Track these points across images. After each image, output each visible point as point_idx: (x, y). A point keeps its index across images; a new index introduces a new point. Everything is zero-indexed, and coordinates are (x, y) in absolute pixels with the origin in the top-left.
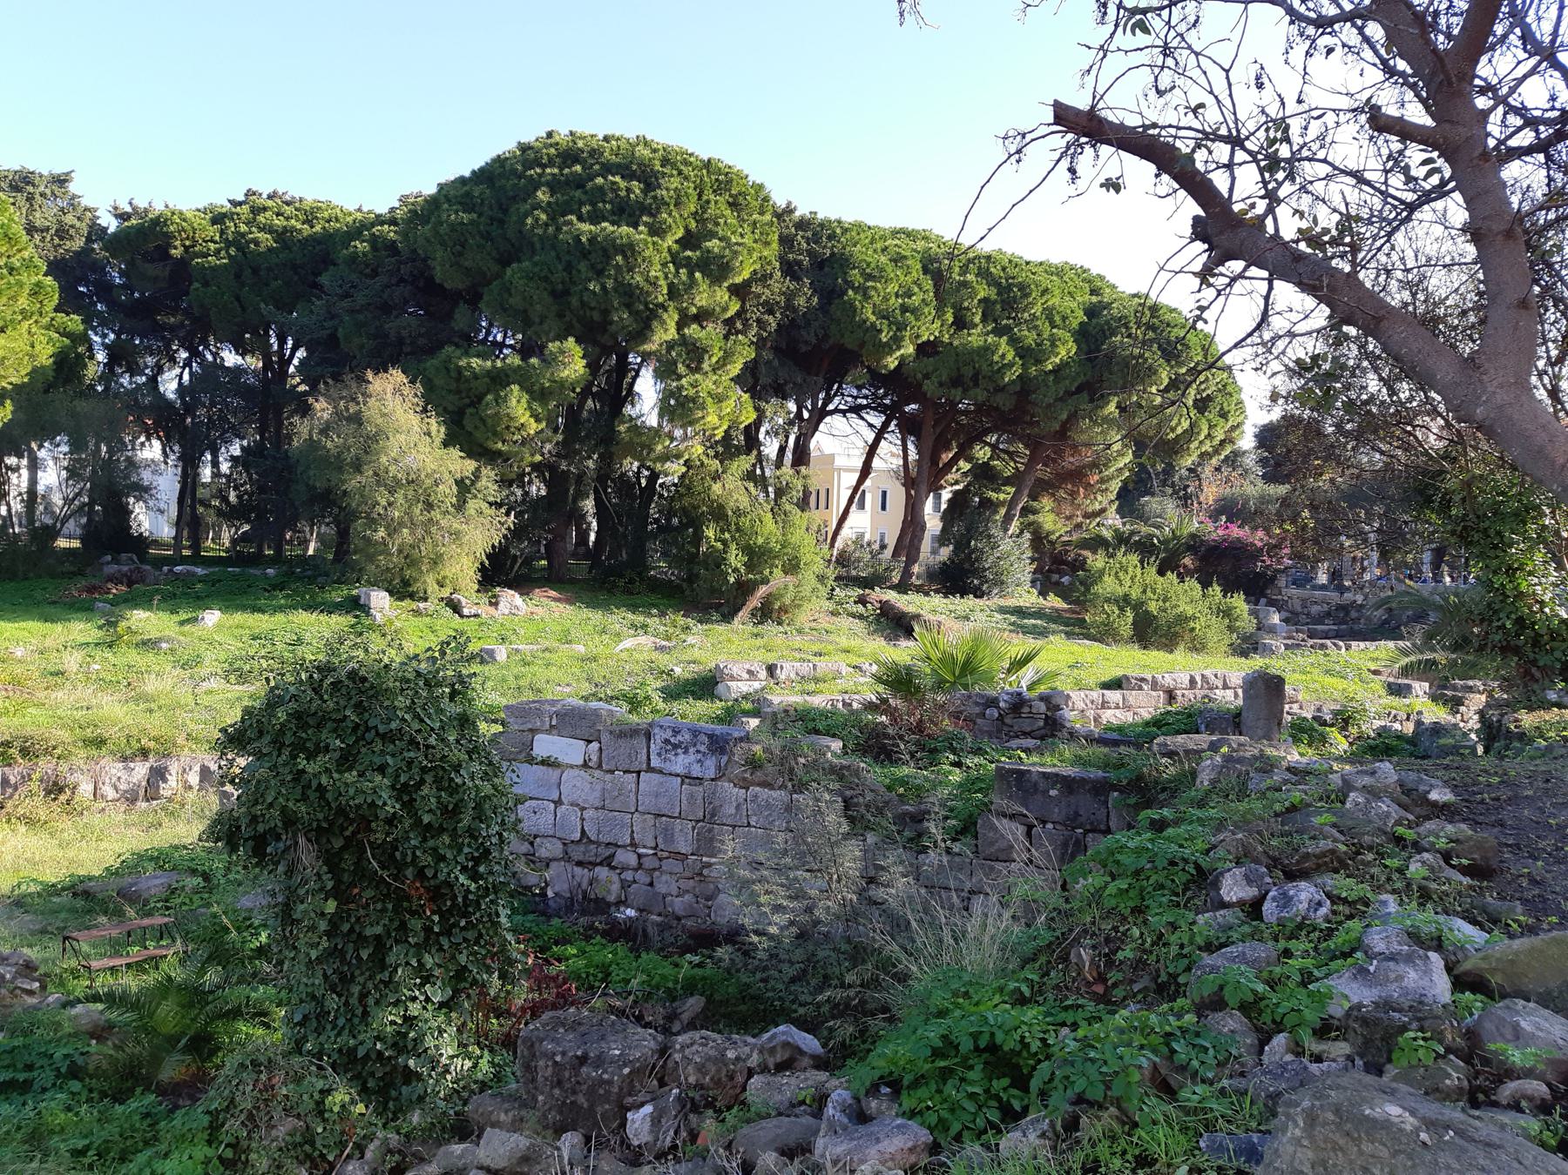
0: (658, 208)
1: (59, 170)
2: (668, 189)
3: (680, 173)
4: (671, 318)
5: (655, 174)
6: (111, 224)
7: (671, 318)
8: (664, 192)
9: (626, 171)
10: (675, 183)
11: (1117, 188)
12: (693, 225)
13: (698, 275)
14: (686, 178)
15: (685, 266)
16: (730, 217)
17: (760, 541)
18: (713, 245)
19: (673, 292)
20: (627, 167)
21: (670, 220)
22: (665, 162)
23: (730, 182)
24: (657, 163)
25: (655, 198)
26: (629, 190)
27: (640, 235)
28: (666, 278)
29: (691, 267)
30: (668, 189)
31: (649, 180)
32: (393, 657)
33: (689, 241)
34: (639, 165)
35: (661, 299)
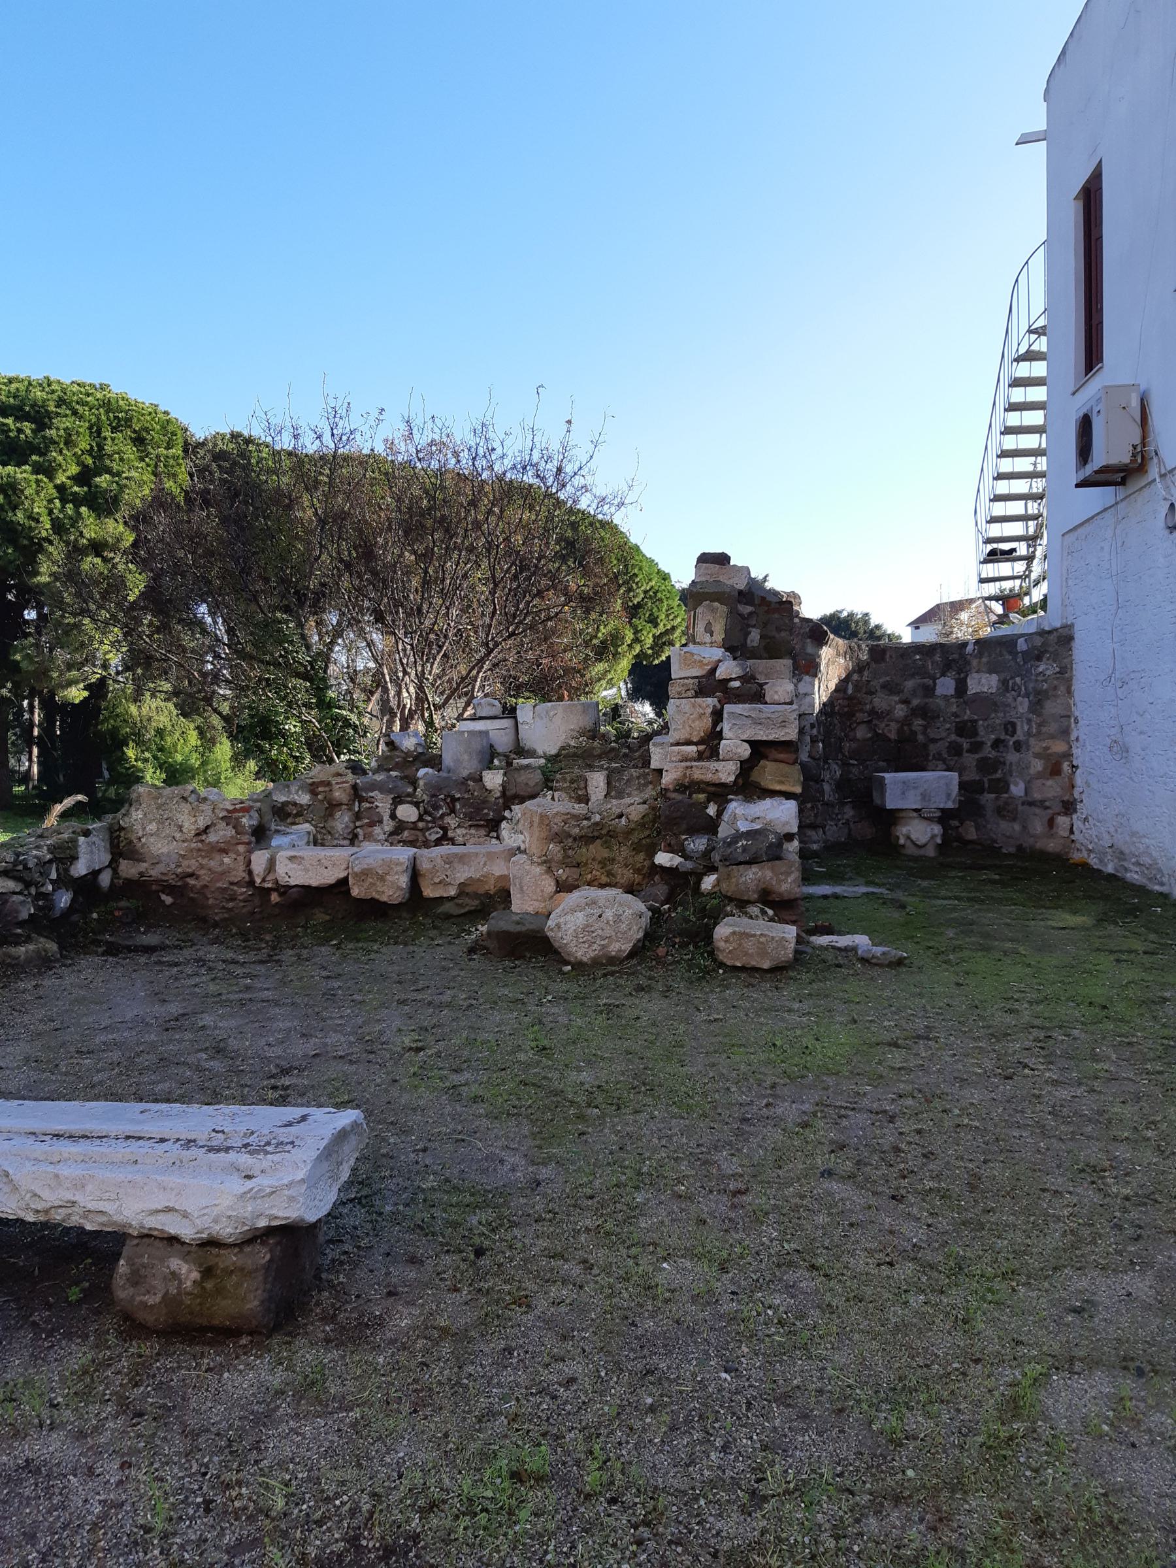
0: (47, 447)
1: (865, 611)
2: (58, 429)
3: (75, 413)
4: (56, 550)
5: (49, 415)
6: (872, 624)
7: (56, 550)
8: (53, 432)
9: (19, 413)
10: (68, 423)
11: (383, 410)
12: (89, 461)
13: (83, 509)
14: (81, 418)
15: (71, 501)
16: (130, 452)
17: (179, 758)
18: (103, 480)
19: (58, 527)
20: (21, 409)
21: (60, 458)
22: (61, 402)
23: (128, 420)
24: (52, 403)
25: (44, 437)
26: (20, 431)
27: (22, 474)
28: (50, 512)
29: (77, 501)
30: (58, 429)
31: (40, 417)
32: (155, 873)
33: (83, 477)
34: (32, 406)
35: (44, 534)
